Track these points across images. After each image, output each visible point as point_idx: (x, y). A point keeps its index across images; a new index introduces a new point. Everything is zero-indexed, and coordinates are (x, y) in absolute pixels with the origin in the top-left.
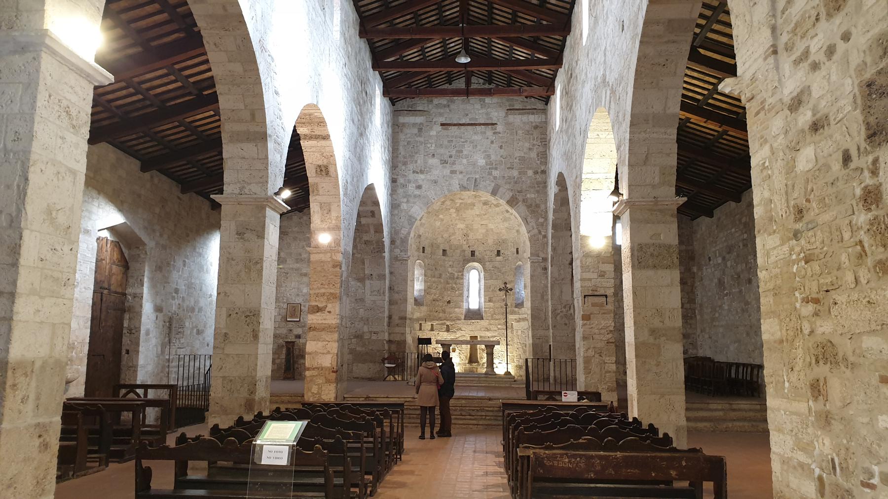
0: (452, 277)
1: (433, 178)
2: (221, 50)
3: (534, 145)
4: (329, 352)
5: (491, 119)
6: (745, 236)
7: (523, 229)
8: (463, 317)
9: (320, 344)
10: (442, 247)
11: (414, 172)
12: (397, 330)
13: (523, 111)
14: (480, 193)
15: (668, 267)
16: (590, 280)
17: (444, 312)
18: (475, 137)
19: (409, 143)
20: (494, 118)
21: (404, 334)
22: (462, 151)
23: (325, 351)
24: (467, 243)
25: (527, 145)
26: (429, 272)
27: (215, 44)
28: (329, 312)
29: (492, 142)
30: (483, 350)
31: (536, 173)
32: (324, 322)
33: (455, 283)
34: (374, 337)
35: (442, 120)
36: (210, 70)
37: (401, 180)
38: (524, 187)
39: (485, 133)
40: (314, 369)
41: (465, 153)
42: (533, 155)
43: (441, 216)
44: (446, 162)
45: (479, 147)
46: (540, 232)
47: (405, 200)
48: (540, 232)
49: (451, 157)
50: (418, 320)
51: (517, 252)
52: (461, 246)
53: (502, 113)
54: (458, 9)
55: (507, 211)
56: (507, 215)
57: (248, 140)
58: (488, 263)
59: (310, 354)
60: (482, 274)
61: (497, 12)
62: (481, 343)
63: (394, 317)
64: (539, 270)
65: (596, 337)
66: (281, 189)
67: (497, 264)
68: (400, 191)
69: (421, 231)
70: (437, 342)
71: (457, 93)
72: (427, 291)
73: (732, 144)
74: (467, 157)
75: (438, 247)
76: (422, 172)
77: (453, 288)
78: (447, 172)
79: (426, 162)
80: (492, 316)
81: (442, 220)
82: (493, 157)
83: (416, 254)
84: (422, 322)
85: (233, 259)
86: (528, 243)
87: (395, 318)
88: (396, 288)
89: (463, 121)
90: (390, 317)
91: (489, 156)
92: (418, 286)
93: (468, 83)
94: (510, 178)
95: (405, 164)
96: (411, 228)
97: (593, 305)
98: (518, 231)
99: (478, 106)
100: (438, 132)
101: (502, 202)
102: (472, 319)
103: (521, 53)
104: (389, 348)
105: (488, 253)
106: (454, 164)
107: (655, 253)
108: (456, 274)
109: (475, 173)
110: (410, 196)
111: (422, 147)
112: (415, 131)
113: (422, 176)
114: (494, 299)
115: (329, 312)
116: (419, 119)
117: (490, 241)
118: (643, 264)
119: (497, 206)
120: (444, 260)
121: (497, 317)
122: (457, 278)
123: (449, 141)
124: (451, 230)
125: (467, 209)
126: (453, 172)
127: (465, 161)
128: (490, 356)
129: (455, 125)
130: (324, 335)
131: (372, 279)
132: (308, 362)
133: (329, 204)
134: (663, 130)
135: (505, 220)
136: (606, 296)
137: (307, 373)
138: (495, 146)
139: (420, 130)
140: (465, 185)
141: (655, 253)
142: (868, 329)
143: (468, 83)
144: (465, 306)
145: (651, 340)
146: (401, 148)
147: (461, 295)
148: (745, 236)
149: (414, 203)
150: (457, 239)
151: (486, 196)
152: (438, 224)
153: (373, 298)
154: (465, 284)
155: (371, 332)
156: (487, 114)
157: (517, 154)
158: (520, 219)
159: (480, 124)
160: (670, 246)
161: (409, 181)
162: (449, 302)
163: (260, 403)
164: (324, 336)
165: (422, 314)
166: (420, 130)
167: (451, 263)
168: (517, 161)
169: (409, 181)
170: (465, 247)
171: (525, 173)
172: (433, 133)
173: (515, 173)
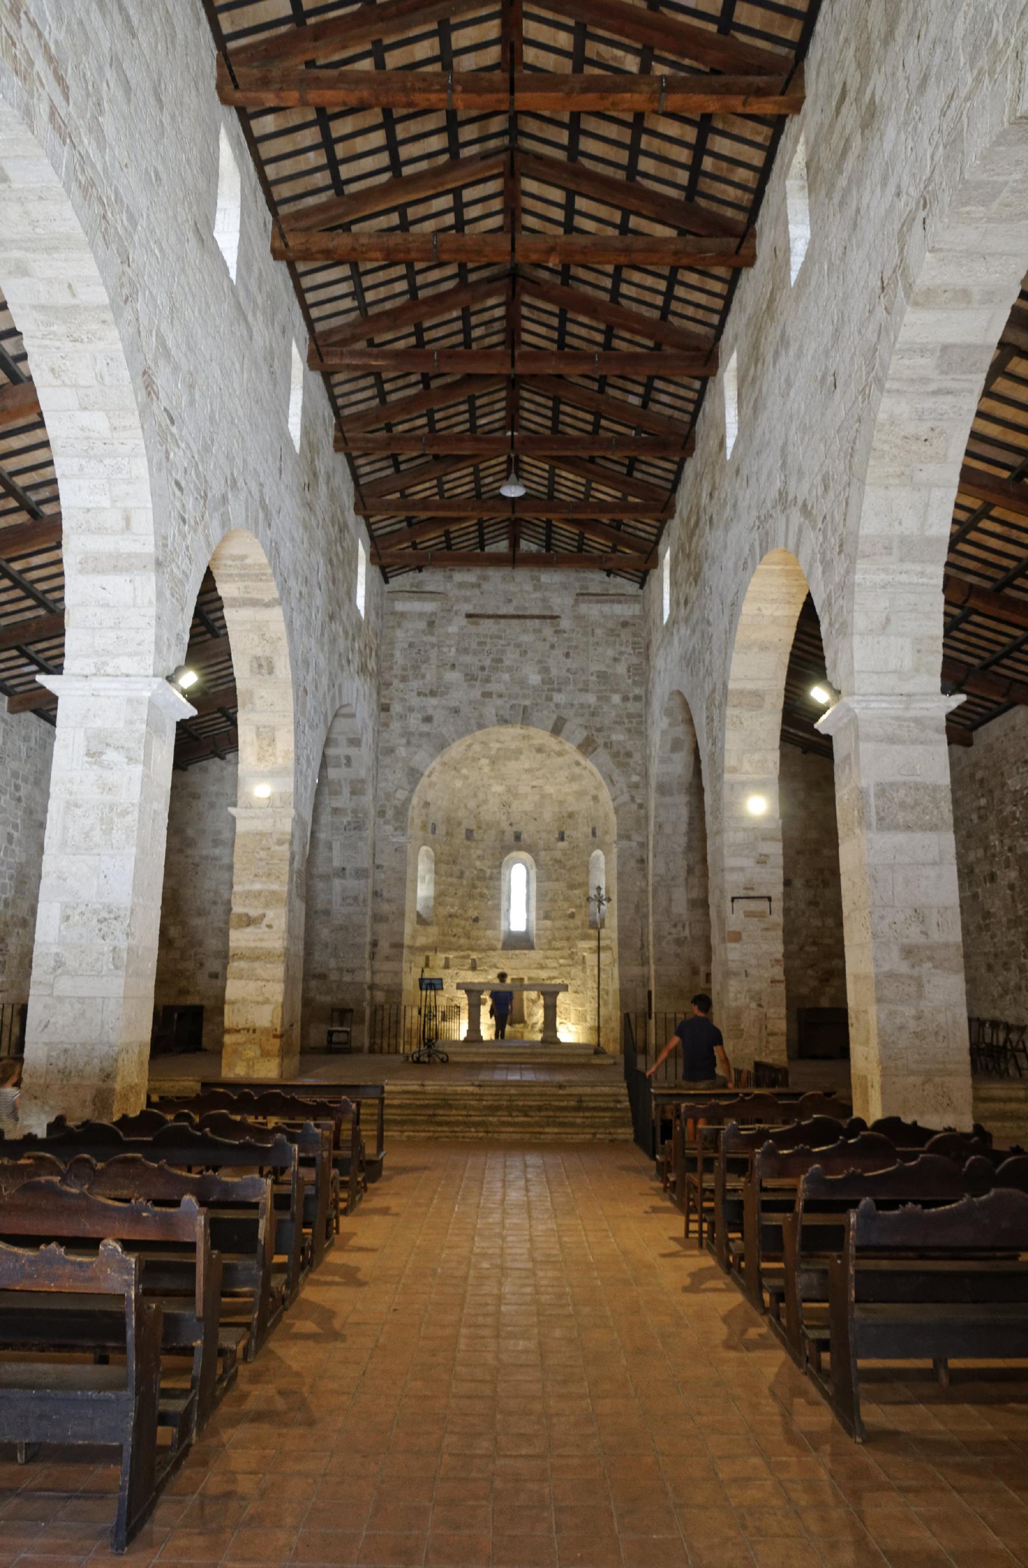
0: (481, 876)
1: (453, 704)
2: (64, 384)
3: (622, 653)
4: (267, 1001)
5: (550, 608)
6: (983, 802)
7: (605, 794)
8: (500, 945)
9: (252, 985)
10: (465, 824)
11: (419, 694)
12: (387, 966)
13: (602, 597)
14: (532, 731)
15: (934, 828)
16: (742, 869)
18: (526, 638)
20: (556, 608)
21: (398, 973)
22: (501, 661)
23: (260, 999)
24: (508, 818)
25: (610, 653)
26: (444, 867)
27: (53, 370)
28: (270, 926)
29: (552, 647)
30: (534, 1002)
31: (626, 699)
32: (259, 944)
33: (487, 887)
34: (347, 978)
35: (469, 608)
36: (50, 463)
37: (397, 708)
38: (606, 722)
39: (540, 631)
40: (238, 1031)
41: (507, 663)
42: (621, 669)
43: (464, 771)
45: (530, 654)
46: (633, 799)
48: (633, 799)
50: (423, 949)
51: (594, 833)
52: (499, 823)
53: (569, 601)
54: (503, 404)
55: (578, 764)
56: (577, 770)
57: (116, 569)
58: (542, 853)
59: (233, 1003)
60: (533, 872)
61: (568, 420)
62: (530, 988)
63: (381, 943)
64: (633, 863)
65: (753, 971)
66: (178, 670)
67: (558, 855)
69: (430, 797)
70: (459, 987)
71: (497, 561)
72: (440, 897)
73: (973, 640)
74: (510, 669)
75: (460, 824)
76: (433, 694)
77: (482, 896)
78: (476, 693)
79: (440, 678)
80: (550, 942)
81: (466, 778)
82: (554, 672)
83: (421, 834)
85: (76, 806)
86: (613, 818)
87: (384, 946)
88: (385, 894)
90: (375, 944)
91: (546, 670)
92: (424, 890)
93: (514, 544)
94: (582, 706)
96: (412, 791)
97: (749, 914)
98: (595, 798)
99: (528, 587)
100: (462, 628)
101: (570, 747)
103: (605, 493)
104: (372, 998)
105: (544, 835)
106: (487, 680)
107: (910, 801)
108: (489, 871)
109: (525, 697)
110: (412, 734)
111: (433, 654)
112: (422, 625)
113: (434, 701)
114: (553, 914)
115: (270, 926)
117: (548, 815)
118: (888, 820)
119: (560, 754)
120: (468, 848)
121: (558, 944)
122: (491, 878)
123: (480, 644)
124: (481, 796)
125: (509, 759)
126: (487, 695)
127: (506, 677)
128: (551, 1011)
129: (489, 617)
130: (259, 968)
131: (344, 877)
132: (230, 1019)
133: (273, 729)
134: (918, 568)
135: (573, 778)
136: (769, 899)
137: (228, 1039)
138: (558, 652)
140: (508, 717)
141: (910, 801)
143: (514, 544)
145: (904, 968)
147: (497, 907)
148: (983, 802)
149: (419, 746)
150: (491, 811)
151: (541, 736)
152: (459, 784)
153: (344, 910)
154: (504, 889)
155: (340, 970)
156: (544, 600)
157: (595, 667)
158: (599, 776)
159: (532, 617)
160: (936, 788)
161: (411, 710)
162: (476, 920)
163: (125, 1097)
164: (259, 972)
165: (430, 940)
166: (431, 624)
167: (479, 852)
168: (594, 678)
169: (411, 710)
170: (505, 825)
171: (607, 700)
172: (453, 629)
173: (591, 699)
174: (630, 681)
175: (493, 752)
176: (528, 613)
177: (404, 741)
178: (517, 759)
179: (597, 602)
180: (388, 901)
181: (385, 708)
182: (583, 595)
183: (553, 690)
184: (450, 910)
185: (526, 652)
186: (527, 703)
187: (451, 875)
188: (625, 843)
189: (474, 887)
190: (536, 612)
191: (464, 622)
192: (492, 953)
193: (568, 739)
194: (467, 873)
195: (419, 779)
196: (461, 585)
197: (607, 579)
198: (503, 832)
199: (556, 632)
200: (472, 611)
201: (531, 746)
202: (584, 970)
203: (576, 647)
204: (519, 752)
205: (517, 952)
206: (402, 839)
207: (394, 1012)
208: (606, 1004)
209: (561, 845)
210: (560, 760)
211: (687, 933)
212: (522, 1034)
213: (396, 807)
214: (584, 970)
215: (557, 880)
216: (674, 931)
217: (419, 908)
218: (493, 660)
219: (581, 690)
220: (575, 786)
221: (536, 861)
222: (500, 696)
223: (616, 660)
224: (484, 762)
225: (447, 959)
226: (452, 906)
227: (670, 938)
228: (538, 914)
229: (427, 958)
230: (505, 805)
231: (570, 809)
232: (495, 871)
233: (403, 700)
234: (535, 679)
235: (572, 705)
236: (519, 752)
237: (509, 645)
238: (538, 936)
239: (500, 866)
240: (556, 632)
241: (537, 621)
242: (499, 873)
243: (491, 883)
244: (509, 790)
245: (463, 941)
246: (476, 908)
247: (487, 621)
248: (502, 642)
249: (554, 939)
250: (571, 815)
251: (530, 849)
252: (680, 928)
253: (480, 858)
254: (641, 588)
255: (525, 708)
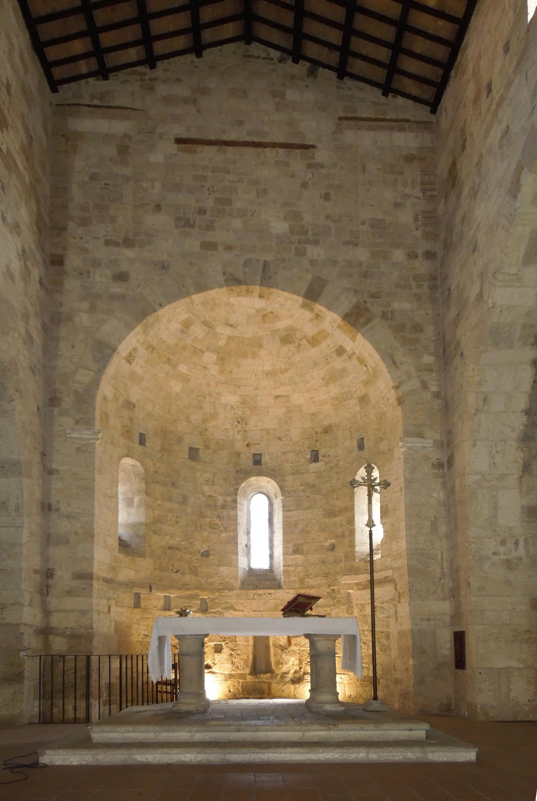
3: (405, 196)
8: (238, 584)
11: (108, 243)
12: (69, 603)
13: (377, 122)
17: (194, 572)
19: (93, 177)
22: (229, 202)
24: (245, 438)
26: (158, 490)
29: (304, 185)
37: (73, 260)
43: (183, 368)
44: (188, 224)
47: (86, 305)
49: (202, 212)
50: (129, 585)
51: (361, 447)
56: (338, 363)
58: (290, 478)
63: (58, 573)
67: (311, 478)
68: (72, 285)
69: (135, 394)
75: (180, 439)
76: (128, 243)
77: (213, 526)
80: (302, 580)
81: (186, 379)
82: (307, 218)
84: (144, 593)
87: (64, 577)
88: (64, 509)
89: (232, 136)
91: (296, 216)
95: (84, 222)
101: (331, 319)
102: (257, 587)
106: (210, 227)
112: (111, 151)
113: (129, 253)
114: (305, 548)
116: (119, 127)
117: (296, 433)
122: (224, 507)
123: (196, 178)
127: (237, 223)
129: (211, 143)
135: (332, 378)
139: (123, 150)
142: (399, 616)
144: (242, 563)
146: (75, 190)
147: (234, 540)
150: (222, 427)
152: (177, 387)
159: (274, 145)
161: (96, 263)
162: (206, 554)
167: (207, 475)
169: (96, 263)
170: (240, 446)
172: (157, 157)
174: (419, 233)
175: (222, 343)
176: (268, 140)
177: (86, 305)
178: (255, 356)
179: (370, 129)
180: (68, 517)
181: (56, 261)
182: (349, 119)
183: (307, 242)
184: (167, 540)
185: (265, 191)
186: (269, 257)
187: (170, 500)
188: (416, 443)
189: (202, 515)
190: (281, 139)
191: (174, 147)
192: (227, 593)
193: (329, 307)
194: (192, 500)
195: (110, 356)
196: (168, 100)
197: (383, 99)
198: (238, 454)
199: (310, 166)
200: (185, 135)
201: (274, 332)
202: (349, 610)
203: (339, 187)
204: (257, 343)
205: (260, 592)
206: (86, 435)
207: (82, 664)
208: (385, 649)
209: (314, 466)
210: (314, 352)
211: (521, 551)
212: (269, 684)
213: (76, 392)
214: (349, 610)
215: (310, 508)
216: (502, 549)
217: (121, 531)
218: (218, 201)
219: (347, 243)
220: (334, 390)
221: (281, 488)
222: (229, 248)
223: (397, 205)
224: (210, 357)
225: (167, 599)
226: (173, 536)
227: (495, 558)
228: (285, 548)
229: (138, 596)
230: (241, 421)
231: (325, 423)
232: (229, 499)
233: (84, 250)
234: (279, 227)
235: (335, 263)
236: (257, 343)
237: (241, 181)
238: (286, 572)
239: (236, 494)
240: (310, 166)
241: (281, 151)
242: (235, 501)
243: (225, 513)
244: (244, 402)
245: (188, 578)
246: (204, 541)
247: (207, 148)
248: (231, 177)
249: (308, 576)
250: (327, 430)
251: (273, 474)
252: (510, 545)
253: (210, 482)
254: (434, 111)
255: (266, 264)
